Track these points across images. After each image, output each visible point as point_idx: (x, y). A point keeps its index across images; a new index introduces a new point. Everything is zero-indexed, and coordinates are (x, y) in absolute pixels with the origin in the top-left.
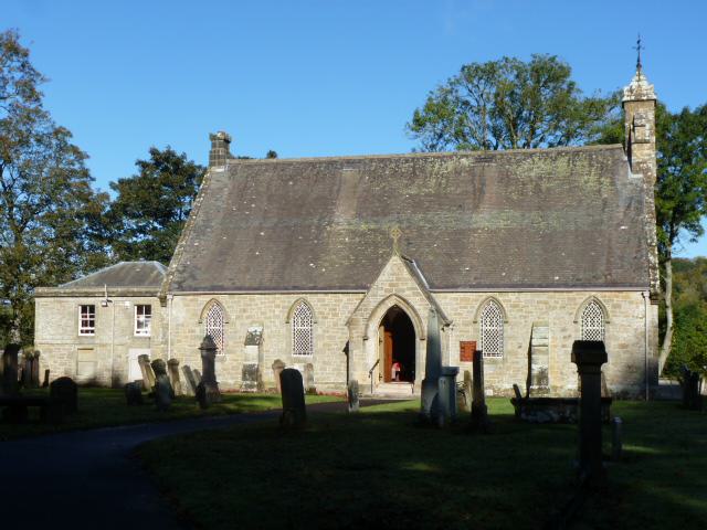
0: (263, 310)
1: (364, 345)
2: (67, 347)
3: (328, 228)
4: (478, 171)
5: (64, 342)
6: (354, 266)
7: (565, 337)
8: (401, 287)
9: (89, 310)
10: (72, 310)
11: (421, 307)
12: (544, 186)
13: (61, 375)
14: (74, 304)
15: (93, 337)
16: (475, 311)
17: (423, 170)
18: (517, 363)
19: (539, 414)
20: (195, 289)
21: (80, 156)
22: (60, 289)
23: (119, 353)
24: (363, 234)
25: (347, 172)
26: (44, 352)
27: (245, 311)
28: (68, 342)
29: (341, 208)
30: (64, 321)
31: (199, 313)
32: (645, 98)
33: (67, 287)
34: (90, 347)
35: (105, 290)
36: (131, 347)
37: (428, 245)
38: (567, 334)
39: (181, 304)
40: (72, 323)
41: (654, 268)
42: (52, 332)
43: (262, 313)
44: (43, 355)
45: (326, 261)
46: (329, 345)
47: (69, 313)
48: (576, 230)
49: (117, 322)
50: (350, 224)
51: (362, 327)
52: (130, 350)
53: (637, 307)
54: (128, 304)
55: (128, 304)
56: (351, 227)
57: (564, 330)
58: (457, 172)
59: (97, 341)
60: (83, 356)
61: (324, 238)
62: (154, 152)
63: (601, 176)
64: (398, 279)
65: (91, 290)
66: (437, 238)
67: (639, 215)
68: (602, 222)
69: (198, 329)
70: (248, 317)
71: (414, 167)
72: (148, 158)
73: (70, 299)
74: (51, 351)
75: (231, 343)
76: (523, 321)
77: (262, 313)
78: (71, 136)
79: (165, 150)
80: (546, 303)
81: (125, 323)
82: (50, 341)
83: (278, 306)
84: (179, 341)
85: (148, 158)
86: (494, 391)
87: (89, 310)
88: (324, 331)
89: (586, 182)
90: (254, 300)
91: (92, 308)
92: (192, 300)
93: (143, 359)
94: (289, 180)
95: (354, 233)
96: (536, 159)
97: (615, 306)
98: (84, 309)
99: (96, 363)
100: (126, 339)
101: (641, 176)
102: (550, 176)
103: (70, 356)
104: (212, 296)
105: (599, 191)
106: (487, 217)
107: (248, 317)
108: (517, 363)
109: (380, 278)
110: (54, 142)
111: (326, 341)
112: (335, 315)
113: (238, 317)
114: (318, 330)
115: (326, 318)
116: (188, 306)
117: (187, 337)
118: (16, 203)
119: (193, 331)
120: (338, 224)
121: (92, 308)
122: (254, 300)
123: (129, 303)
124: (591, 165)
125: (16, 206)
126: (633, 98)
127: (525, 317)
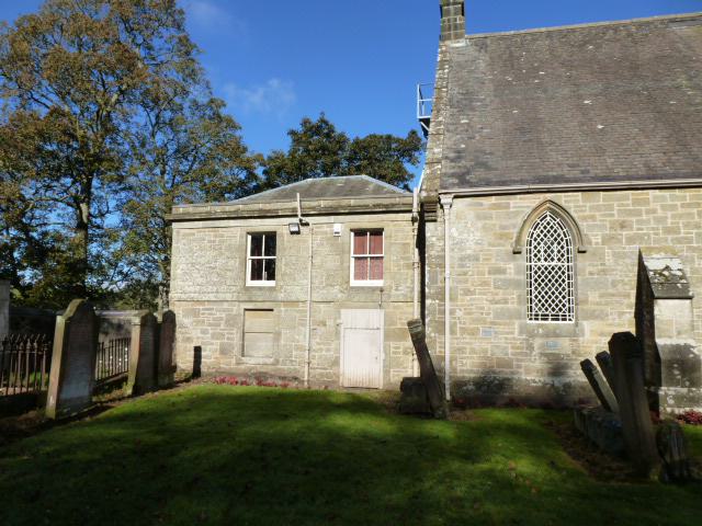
0: (660, 213)
2: (225, 305)
5: (221, 296)
9: (264, 243)
10: (237, 241)
13: (607, 345)
14: (237, 234)
15: (271, 289)
20: (503, 188)
21: (232, 125)
23: (320, 317)
27: (623, 226)
28: (228, 297)
30: (221, 261)
31: (515, 232)
35: (297, 204)
36: (343, 305)
39: (471, 214)
42: (200, 280)
44: (179, 319)
47: (229, 248)
49: (317, 261)
52: (343, 311)
54: (337, 227)
59: (281, 296)
60: (255, 322)
62: (305, 122)
69: (511, 267)
70: (631, 240)
72: (299, 129)
73: (232, 223)
74: (195, 313)
75: (593, 296)
77: (668, 231)
78: (225, 105)
81: (332, 262)
82: (196, 296)
84: (467, 292)
85: (299, 129)
87: (264, 243)
90: (646, 202)
91: (272, 237)
94: (586, 43)
98: (256, 238)
99: (278, 335)
100: (335, 292)
103: (231, 321)
104: (543, 197)
110: (208, 112)
113: (607, 240)
117: (485, 283)
119: (502, 271)
121: (272, 237)
122: (646, 202)
123: (340, 226)
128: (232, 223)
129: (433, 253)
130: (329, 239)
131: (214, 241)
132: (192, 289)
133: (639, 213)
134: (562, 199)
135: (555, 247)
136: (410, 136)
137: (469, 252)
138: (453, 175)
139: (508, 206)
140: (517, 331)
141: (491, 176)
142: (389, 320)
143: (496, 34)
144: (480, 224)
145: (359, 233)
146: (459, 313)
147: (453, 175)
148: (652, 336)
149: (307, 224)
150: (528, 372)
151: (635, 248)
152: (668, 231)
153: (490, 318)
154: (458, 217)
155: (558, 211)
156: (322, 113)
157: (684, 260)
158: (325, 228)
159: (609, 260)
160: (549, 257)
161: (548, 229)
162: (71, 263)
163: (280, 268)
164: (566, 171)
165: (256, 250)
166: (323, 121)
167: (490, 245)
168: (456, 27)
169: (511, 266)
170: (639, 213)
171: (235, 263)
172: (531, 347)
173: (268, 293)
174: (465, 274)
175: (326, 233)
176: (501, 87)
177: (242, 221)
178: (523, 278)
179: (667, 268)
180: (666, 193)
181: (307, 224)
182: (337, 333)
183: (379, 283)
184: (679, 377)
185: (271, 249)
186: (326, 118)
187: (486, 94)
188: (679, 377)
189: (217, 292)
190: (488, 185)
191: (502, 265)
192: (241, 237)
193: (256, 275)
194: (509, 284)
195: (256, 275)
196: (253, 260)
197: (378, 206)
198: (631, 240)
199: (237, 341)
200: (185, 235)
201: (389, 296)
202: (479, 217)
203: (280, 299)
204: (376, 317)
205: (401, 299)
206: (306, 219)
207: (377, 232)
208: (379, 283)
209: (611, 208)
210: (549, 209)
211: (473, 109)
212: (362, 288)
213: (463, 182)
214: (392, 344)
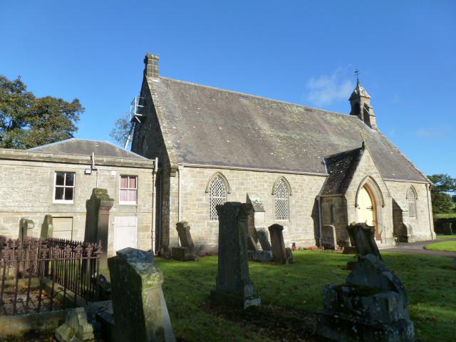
5: (36, 209)
14: (49, 172)
15: (71, 205)
22: (33, 152)
27: (242, 184)
31: (206, 183)
33: (41, 151)
42: (19, 199)
43: (255, 187)
46: (300, 212)
47: (42, 180)
52: (115, 217)
54: (113, 173)
55: (113, 173)
65: (71, 157)
82: (16, 209)
83: (266, 182)
84: (187, 209)
88: (296, 202)
92: (199, 172)
109: (171, 182)
111: (298, 209)
112: (302, 190)
113: (238, 189)
114: (293, 201)
115: (297, 192)
116: (196, 177)
117: (194, 205)
118: (27, 287)
119: (201, 200)
125: (30, 280)
128: (45, 164)
129: (173, 191)
130: (107, 179)
131: (30, 175)
132: (12, 204)
133: (247, 180)
134: (223, 172)
135: (219, 191)
136: (74, 102)
137: (188, 191)
138: (179, 156)
139: (203, 173)
140: (206, 225)
141: (195, 158)
142: (140, 222)
143: (173, 80)
144: (193, 179)
145: (124, 176)
147: (179, 156)
148: (253, 225)
149: (96, 170)
150: (210, 241)
151: (245, 193)
152: (255, 187)
153: (196, 220)
154: (184, 176)
155: (221, 176)
156: (19, 77)
157: (261, 198)
158: (106, 173)
161: (217, 184)
164: (222, 160)
165: (60, 181)
166: (19, 82)
167: (197, 188)
168: (155, 71)
169: (205, 198)
170: (247, 180)
171: (46, 189)
172: (211, 232)
173: (70, 208)
174: (186, 201)
175: (106, 175)
176: (184, 112)
177: (53, 164)
178: (208, 203)
179: (256, 201)
180: (255, 173)
181: (96, 170)
185: (70, 182)
186: (21, 80)
187: (178, 114)
189: (32, 206)
190: (196, 163)
191: (201, 197)
192: (51, 173)
193: (58, 196)
194: (204, 205)
195: (58, 196)
196: (57, 188)
197: (136, 164)
198: (244, 189)
200: (6, 169)
201: (141, 210)
202: (192, 176)
203: (77, 211)
204: (133, 220)
205: (146, 211)
206: (97, 167)
207: (133, 177)
210: (219, 176)
211: (176, 122)
212: (126, 206)
213: (186, 161)
214: (141, 234)
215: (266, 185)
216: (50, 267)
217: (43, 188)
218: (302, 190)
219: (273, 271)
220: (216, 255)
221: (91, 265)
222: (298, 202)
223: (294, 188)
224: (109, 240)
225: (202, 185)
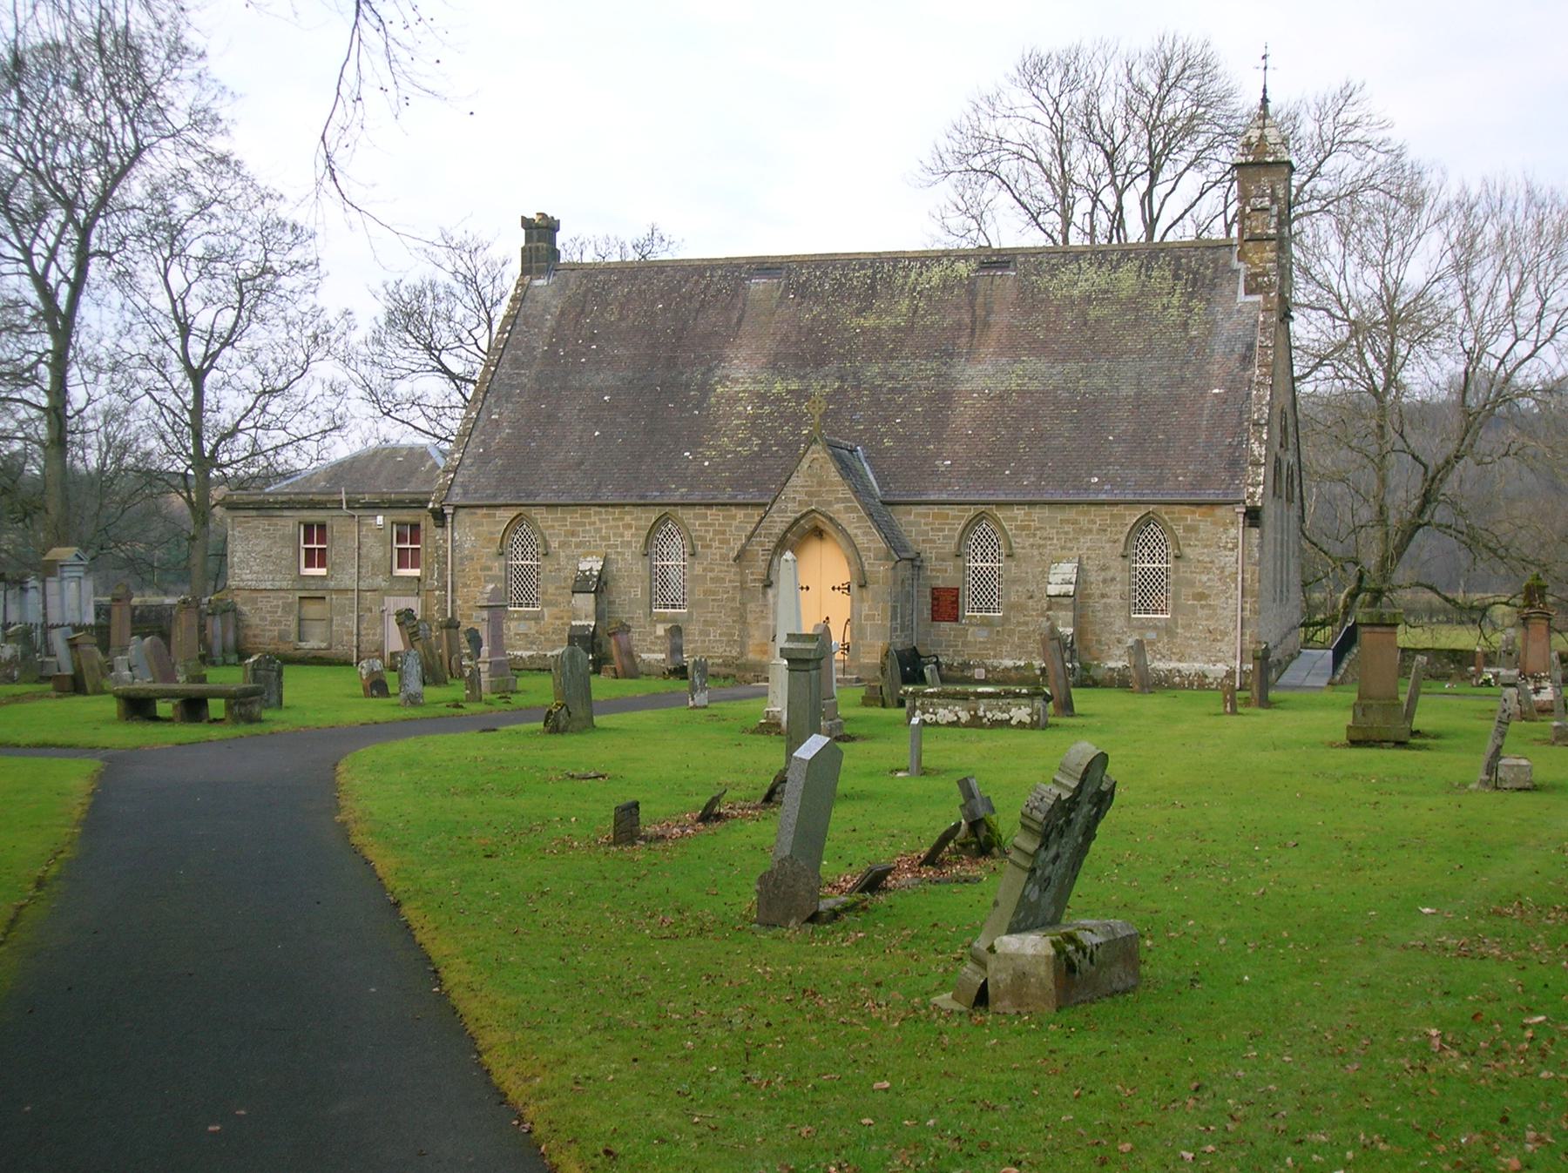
1: (765, 594)
3: (720, 390)
4: (982, 285)
5: (278, 585)
6: (757, 455)
7: (1104, 581)
8: (825, 497)
11: (859, 532)
12: (1093, 313)
16: (957, 535)
17: (889, 283)
18: (1026, 624)
19: (941, 711)
24: (779, 399)
25: (758, 285)
26: (244, 604)
27: (573, 534)
28: (284, 584)
29: (743, 353)
32: (1270, 159)
34: (319, 594)
37: (886, 420)
38: (1110, 574)
40: (289, 552)
41: (1257, 464)
42: (255, 568)
45: (709, 447)
46: (714, 593)
47: (283, 537)
48: (1138, 396)
50: (756, 381)
51: (761, 565)
53: (1226, 530)
56: (759, 387)
57: (1104, 568)
58: (945, 286)
59: (332, 584)
60: (312, 610)
61: (709, 407)
63: (1191, 296)
64: (820, 484)
66: (902, 408)
67: (1244, 370)
68: (1183, 380)
70: (578, 545)
71: (873, 278)
75: (551, 590)
76: (1036, 552)
77: (603, 538)
79: (288, 695)
80: (1075, 522)
82: (253, 584)
83: (629, 526)
84: (465, 585)
86: (987, 671)
89: (1165, 308)
93: (405, 617)
95: (763, 398)
96: (1084, 265)
97: (1188, 529)
98: (309, 528)
101: (1258, 298)
102: (1104, 296)
105: (1185, 325)
106: (991, 370)
107: (578, 545)
108: (1026, 624)
111: (709, 585)
113: (562, 545)
115: (710, 547)
117: (478, 578)
119: (490, 569)
120: (736, 381)
124: (1176, 277)
126: (1251, 158)
127: (1040, 546)
133: (584, 525)
146: (459, 602)
152: (603, 538)
159: (563, 562)
160: (525, 558)
162: (149, 471)
163: (331, 556)
182: (382, 619)
183: (416, 572)
184: (136, 601)
188: (136, 601)
199: (294, 626)
208: (416, 572)
209: (565, 519)
215: (628, 535)
216: (990, 689)
217: (286, 551)
218: (724, 542)
219: (219, 632)
220: (1347, 707)
221: (957, 693)
222: (712, 570)
223: (702, 538)
224: (438, 737)
225: (492, 540)
